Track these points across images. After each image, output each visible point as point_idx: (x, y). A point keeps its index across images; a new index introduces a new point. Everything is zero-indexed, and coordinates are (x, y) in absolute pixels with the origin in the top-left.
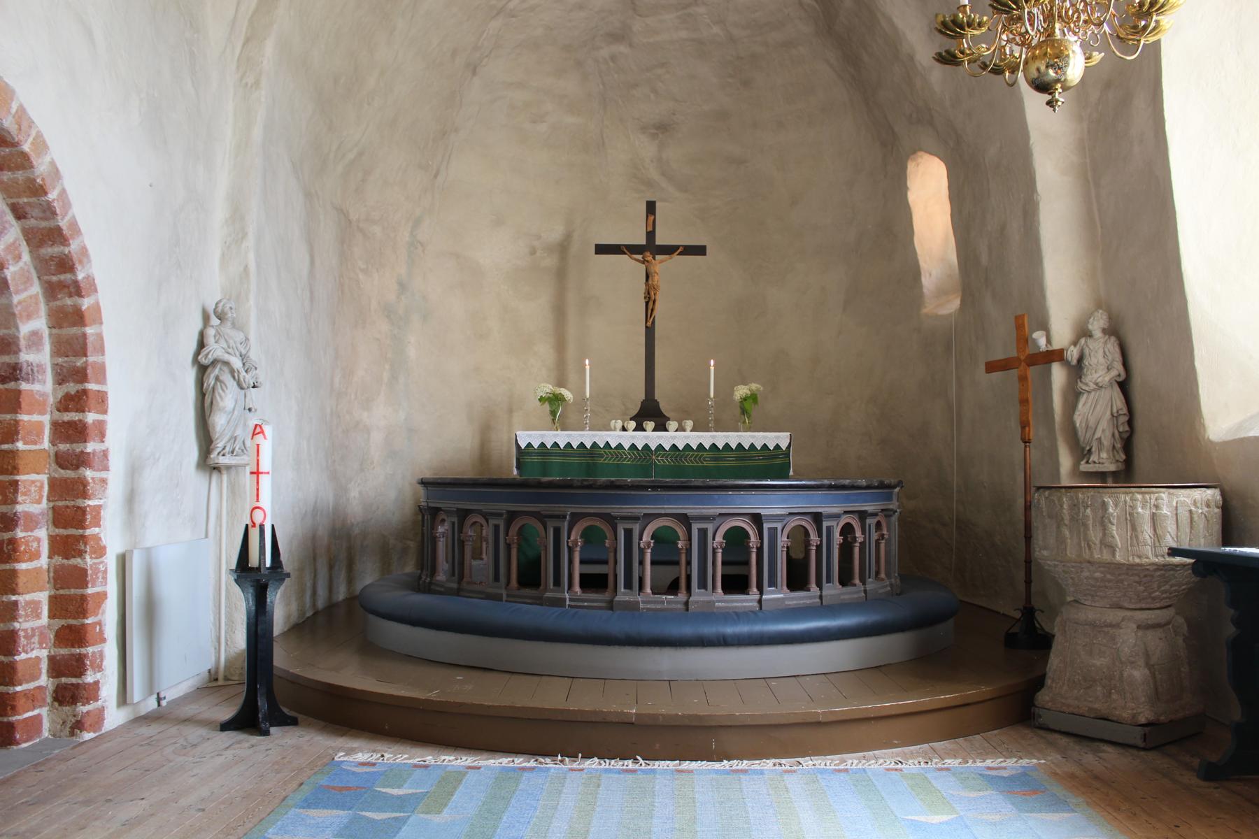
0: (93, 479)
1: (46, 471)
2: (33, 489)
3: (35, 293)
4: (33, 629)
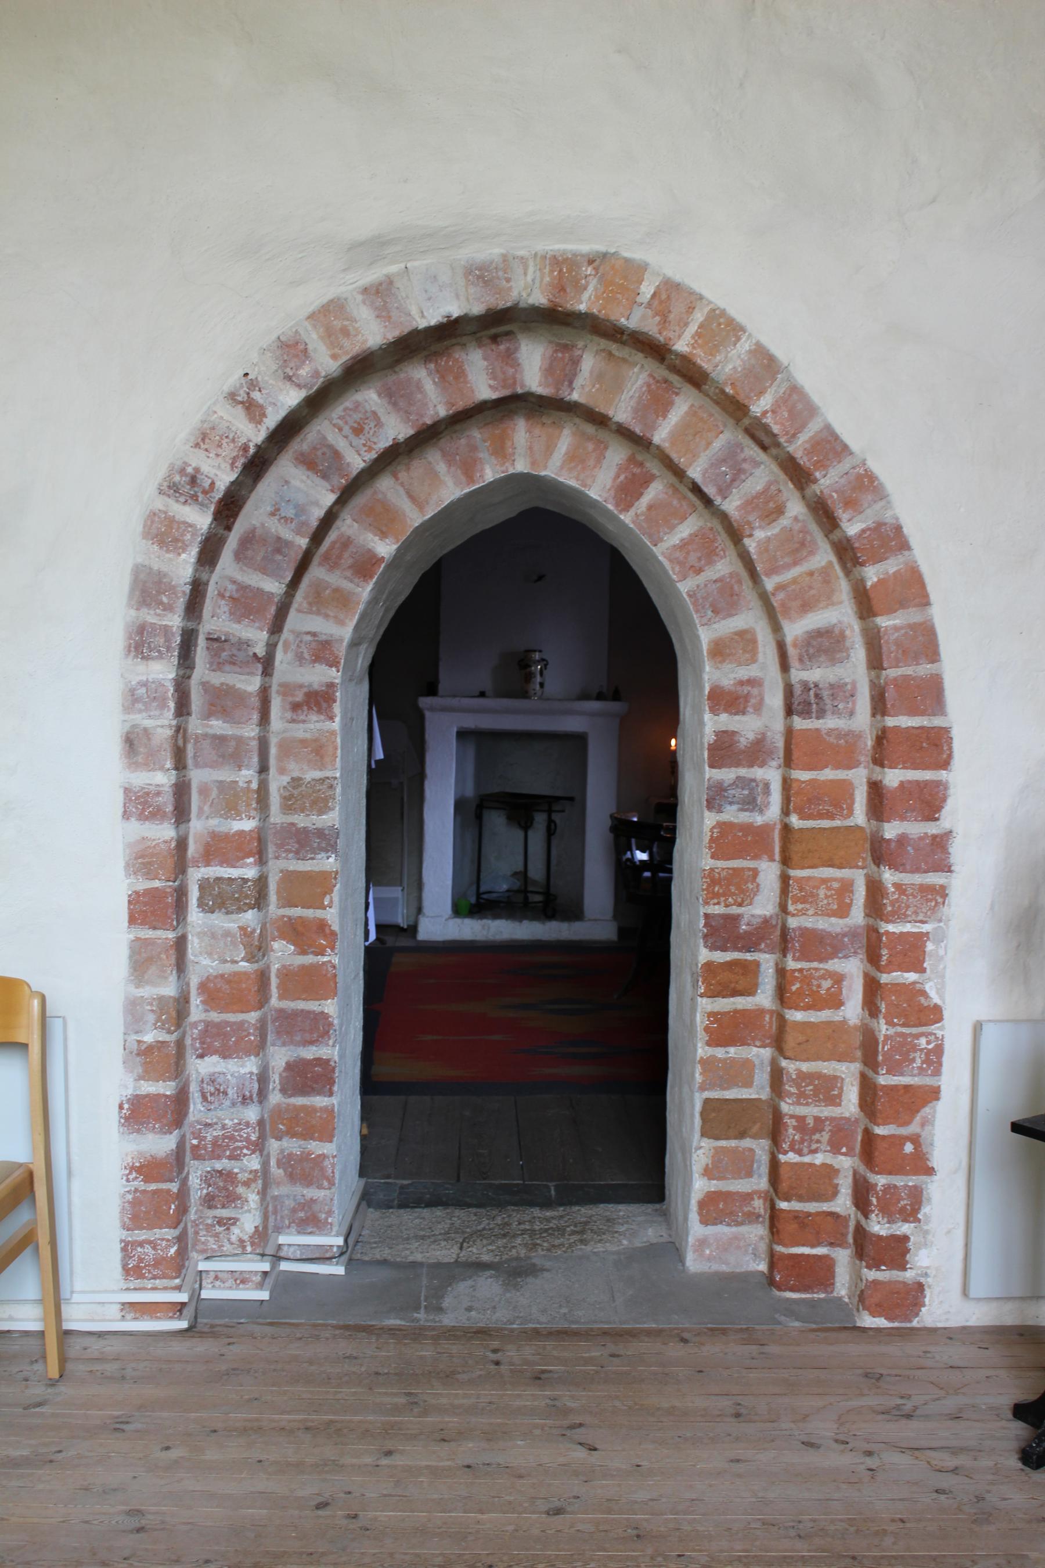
0: (895, 885)
1: (860, 864)
2: (822, 892)
3: (823, 563)
4: (817, 1119)
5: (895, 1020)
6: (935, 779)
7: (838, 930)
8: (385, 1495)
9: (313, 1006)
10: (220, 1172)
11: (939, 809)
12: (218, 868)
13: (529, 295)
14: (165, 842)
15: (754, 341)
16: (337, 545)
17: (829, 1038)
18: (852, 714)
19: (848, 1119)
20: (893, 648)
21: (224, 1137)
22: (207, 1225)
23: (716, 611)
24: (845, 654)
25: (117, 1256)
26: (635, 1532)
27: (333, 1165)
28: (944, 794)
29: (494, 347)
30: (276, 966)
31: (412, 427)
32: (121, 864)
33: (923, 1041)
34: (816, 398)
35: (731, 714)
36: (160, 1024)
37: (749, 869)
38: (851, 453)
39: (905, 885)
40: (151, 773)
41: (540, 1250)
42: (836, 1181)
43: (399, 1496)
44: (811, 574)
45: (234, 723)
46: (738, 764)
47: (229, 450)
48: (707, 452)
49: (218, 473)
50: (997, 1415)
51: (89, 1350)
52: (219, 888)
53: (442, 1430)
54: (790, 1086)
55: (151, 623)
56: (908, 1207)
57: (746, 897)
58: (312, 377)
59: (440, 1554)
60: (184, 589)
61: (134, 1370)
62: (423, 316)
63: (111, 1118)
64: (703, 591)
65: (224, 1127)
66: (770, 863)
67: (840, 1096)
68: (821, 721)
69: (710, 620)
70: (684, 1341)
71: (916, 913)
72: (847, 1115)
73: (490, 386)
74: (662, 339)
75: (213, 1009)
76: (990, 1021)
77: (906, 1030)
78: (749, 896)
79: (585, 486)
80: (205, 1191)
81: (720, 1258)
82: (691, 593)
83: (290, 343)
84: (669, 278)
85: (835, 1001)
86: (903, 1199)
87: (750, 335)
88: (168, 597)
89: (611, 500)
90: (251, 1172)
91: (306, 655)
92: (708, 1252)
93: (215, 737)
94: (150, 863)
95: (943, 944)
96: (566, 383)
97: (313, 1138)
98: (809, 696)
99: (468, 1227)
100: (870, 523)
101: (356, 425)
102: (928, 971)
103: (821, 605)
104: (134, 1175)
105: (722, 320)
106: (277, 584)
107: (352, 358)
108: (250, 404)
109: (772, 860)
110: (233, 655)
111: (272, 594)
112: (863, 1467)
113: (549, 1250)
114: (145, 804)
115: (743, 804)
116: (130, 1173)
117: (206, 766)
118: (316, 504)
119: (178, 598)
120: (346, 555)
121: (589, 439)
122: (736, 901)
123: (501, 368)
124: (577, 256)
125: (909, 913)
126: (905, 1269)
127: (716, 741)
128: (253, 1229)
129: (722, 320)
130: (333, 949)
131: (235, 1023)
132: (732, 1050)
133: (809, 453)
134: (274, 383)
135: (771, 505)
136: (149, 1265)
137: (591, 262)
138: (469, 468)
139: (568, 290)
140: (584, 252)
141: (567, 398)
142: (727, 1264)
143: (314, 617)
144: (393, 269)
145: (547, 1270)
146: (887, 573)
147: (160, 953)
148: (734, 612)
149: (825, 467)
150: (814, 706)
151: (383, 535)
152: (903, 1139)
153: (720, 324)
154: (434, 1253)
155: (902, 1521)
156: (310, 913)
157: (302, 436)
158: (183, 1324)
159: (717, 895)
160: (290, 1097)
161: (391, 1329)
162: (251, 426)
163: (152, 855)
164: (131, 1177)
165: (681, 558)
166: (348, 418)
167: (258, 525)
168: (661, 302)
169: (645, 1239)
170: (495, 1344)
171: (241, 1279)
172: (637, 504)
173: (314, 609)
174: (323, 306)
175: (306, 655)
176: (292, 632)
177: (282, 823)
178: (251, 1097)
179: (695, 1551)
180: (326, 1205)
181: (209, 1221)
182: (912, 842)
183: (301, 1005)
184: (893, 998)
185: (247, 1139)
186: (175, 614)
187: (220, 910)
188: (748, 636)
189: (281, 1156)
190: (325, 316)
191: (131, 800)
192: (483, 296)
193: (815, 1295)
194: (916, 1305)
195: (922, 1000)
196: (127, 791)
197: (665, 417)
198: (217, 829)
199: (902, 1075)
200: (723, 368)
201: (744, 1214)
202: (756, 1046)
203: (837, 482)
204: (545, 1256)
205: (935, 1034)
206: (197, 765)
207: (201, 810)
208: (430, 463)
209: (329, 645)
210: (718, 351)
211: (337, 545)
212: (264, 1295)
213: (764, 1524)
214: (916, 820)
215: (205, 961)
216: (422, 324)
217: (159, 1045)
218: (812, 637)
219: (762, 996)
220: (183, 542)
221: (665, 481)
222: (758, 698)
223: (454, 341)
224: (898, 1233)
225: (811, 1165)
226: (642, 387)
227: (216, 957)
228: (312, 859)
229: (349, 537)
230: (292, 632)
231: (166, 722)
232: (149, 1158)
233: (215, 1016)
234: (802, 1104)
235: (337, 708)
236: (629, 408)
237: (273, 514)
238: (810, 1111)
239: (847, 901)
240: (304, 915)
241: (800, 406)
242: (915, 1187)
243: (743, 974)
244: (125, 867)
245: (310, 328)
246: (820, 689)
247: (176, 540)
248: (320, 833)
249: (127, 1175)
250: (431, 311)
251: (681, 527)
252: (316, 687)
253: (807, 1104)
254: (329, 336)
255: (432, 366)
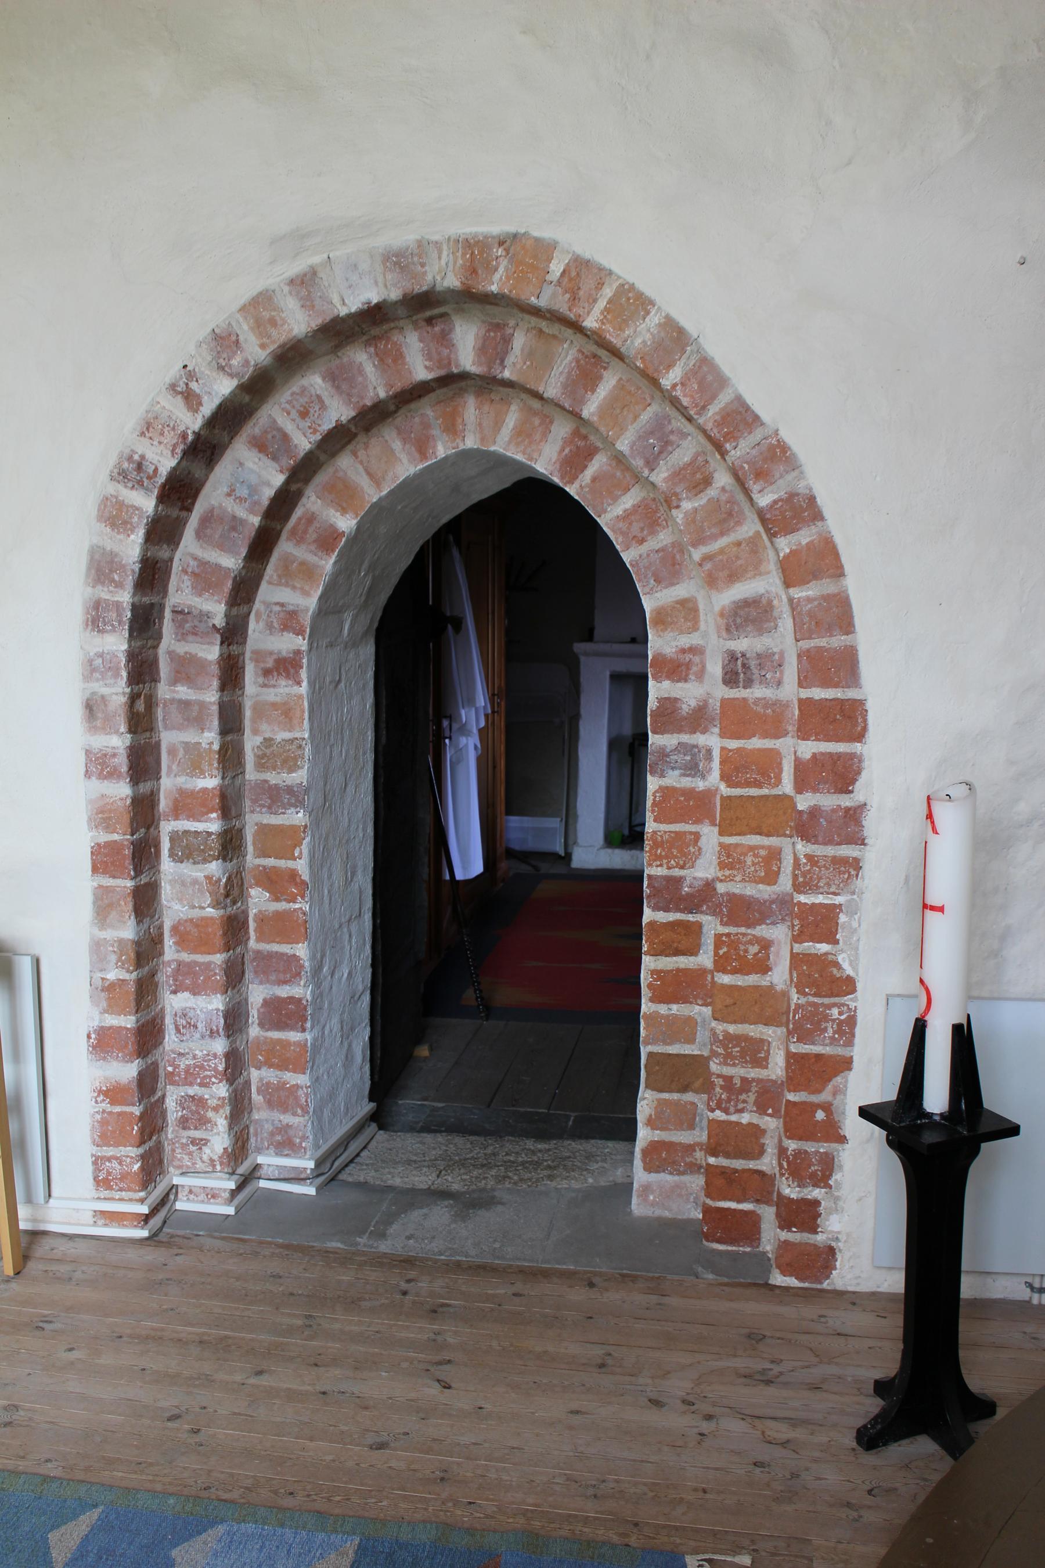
2: (749, 860)
3: (751, 534)
4: (744, 1080)
5: (807, 990)
6: (849, 751)
7: (766, 897)
8: (235, 1414)
9: (285, 949)
10: (192, 1097)
11: (853, 781)
12: (186, 822)
13: (443, 279)
14: (122, 799)
15: (663, 314)
16: (303, 521)
17: (756, 1003)
18: (779, 683)
19: (774, 1082)
20: (806, 619)
21: (195, 1066)
22: (182, 1144)
23: (658, 581)
24: (772, 624)
25: (89, 1168)
26: (442, 1475)
27: (307, 1095)
28: (858, 767)
29: (429, 329)
30: (254, 911)
31: (354, 410)
32: (85, 818)
33: (835, 1011)
34: (726, 369)
35: (673, 681)
36: (120, 964)
37: (691, 833)
38: (762, 424)
39: (817, 856)
40: (108, 736)
41: (507, 1183)
42: (762, 1141)
43: (246, 1415)
44: (739, 544)
45: (198, 689)
46: (680, 730)
47: (170, 438)
48: (634, 425)
49: (160, 459)
50: (859, 1389)
51: (55, 1251)
52: (187, 840)
53: (319, 1354)
54: (717, 1047)
55: (105, 600)
56: (819, 1173)
57: (688, 860)
58: (243, 366)
59: (252, 1477)
60: (133, 567)
61: (83, 1272)
62: (344, 304)
63: (82, 1046)
64: (645, 561)
65: (194, 1057)
66: (712, 828)
67: (766, 1059)
68: (748, 690)
69: (652, 589)
70: (591, 1285)
71: (828, 885)
72: (774, 1077)
73: (426, 367)
74: (572, 316)
75: (184, 949)
76: (899, 996)
77: (816, 1000)
78: (691, 859)
79: (531, 459)
80: (180, 1114)
81: (663, 1204)
82: (634, 563)
83: (224, 335)
84: (578, 256)
85: (764, 968)
86: (814, 1165)
87: (659, 308)
88: (120, 576)
89: (556, 473)
90: (219, 1098)
91: (276, 625)
92: (651, 1198)
93: (181, 702)
94: (110, 818)
95: (856, 917)
96: (498, 361)
97: (287, 1069)
98: (736, 665)
99: (458, 1155)
100: (782, 494)
101: (302, 409)
102: (841, 942)
103: (749, 576)
104: (102, 1097)
105: (630, 295)
106: (233, 560)
107: (279, 347)
108: (189, 394)
109: (713, 824)
110: (195, 626)
111: (229, 569)
112: (696, 1430)
113: (515, 1183)
114: (104, 765)
115: (684, 770)
116: (99, 1095)
117: (173, 728)
118: (268, 484)
119: (128, 576)
120: (311, 530)
121: (535, 413)
122: (678, 864)
123: (436, 349)
124: (488, 238)
125: (821, 884)
126: (816, 1233)
127: (658, 708)
128: (222, 1150)
129: (630, 295)
130: (303, 897)
131: (203, 964)
132: (675, 1008)
133: (719, 425)
134: (209, 373)
135: (698, 476)
136: (116, 1179)
137: (501, 243)
138: (422, 447)
139: (480, 272)
140: (494, 234)
141: (499, 376)
142: (670, 1210)
143: (283, 588)
144: (317, 259)
145: (503, 1204)
146: (800, 544)
147: (119, 900)
148: (675, 582)
149: (736, 439)
150: (742, 675)
151: (344, 511)
152: (814, 1107)
153: (629, 299)
154: (413, 1178)
155: (705, 1491)
156: (282, 863)
157: (254, 421)
158: (145, 1233)
159: (659, 858)
160: (267, 1030)
161: (327, 1252)
162: (189, 414)
163: (110, 811)
164: (99, 1099)
165: (624, 529)
166: (295, 403)
167: (216, 504)
168: (571, 280)
169: (611, 1179)
170: (412, 1274)
171: (212, 1195)
172: (581, 476)
173: (283, 581)
174: (253, 299)
175: (276, 625)
176: (264, 602)
177: (257, 780)
178: (218, 1030)
179: (487, 1500)
180: (301, 1130)
181: (184, 1141)
182: (824, 814)
183: (275, 948)
184: (805, 968)
185: (215, 1069)
186: (125, 591)
187: (188, 860)
188: (690, 605)
189: (260, 1084)
190: (255, 308)
191: (91, 760)
192: (399, 282)
193: (741, 1249)
194: (827, 1267)
195: (835, 971)
196: (88, 752)
197: (593, 391)
198: (184, 786)
199: (813, 1043)
200: (632, 343)
201: (686, 1164)
202: (698, 1005)
203: (748, 453)
204: (508, 1189)
205: (848, 1006)
206: (166, 728)
207: (169, 767)
208: (386, 441)
209: (296, 614)
210: (628, 326)
211: (303, 521)
212: (230, 1210)
213: (568, 1480)
214: (828, 792)
215: (177, 906)
216: (343, 311)
217: (120, 982)
218: (739, 607)
219: (705, 956)
220: (131, 524)
221: (609, 453)
222: (700, 666)
223: (392, 325)
224: (809, 1197)
225: (738, 1124)
226: (571, 363)
227: (185, 903)
228: (284, 813)
229: (313, 513)
230: (264, 602)
231: (120, 690)
232: (114, 1083)
233: (185, 957)
234: (729, 1065)
235: (304, 674)
236: (559, 384)
237: (229, 495)
238: (738, 1072)
239: (775, 868)
240: (277, 865)
241: (710, 378)
242: (826, 1153)
243: (685, 935)
244: (88, 821)
245: (241, 320)
246: (747, 659)
247: (125, 523)
248: (290, 790)
249: (96, 1098)
250: (352, 298)
251: (624, 499)
252: (284, 654)
253: (734, 1065)
254: (259, 327)
255: (372, 350)
